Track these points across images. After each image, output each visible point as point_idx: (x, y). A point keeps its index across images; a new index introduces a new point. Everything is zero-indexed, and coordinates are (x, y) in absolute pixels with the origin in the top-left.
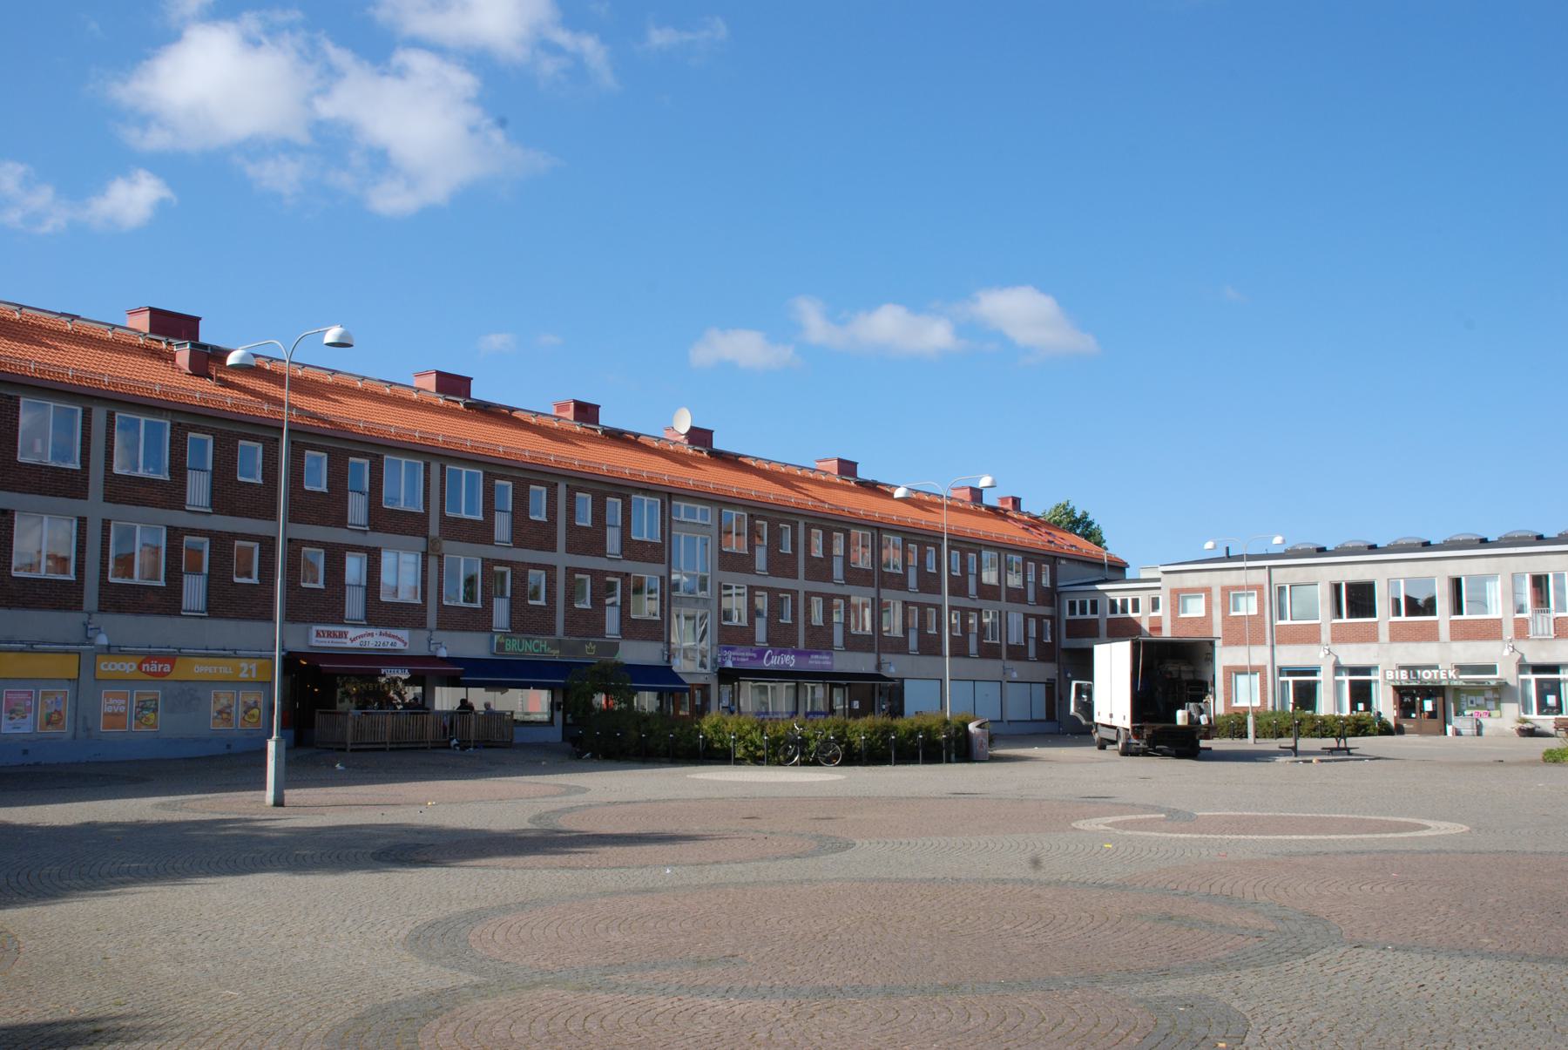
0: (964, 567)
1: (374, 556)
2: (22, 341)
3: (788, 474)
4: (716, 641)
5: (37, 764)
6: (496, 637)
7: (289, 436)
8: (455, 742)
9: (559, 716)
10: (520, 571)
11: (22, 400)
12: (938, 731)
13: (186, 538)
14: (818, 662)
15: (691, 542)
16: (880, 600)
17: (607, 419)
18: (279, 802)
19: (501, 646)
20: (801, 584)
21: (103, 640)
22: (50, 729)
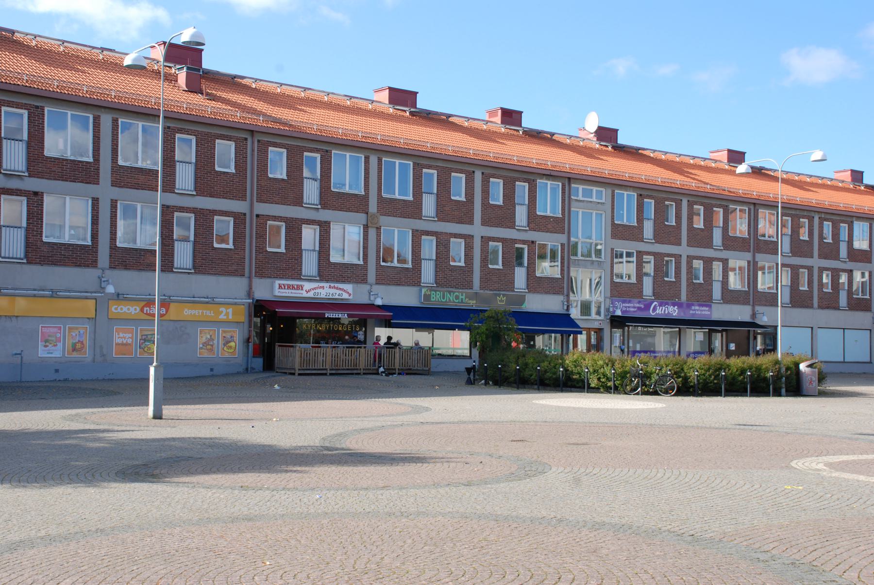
0: (836, 235)
1: (325, 228)
2: (279, 106)
3: (681, 163)
4: (609, 295)
5: (66, 380)
6: (424, 290)
7: (164, 122)
8: (382, 369)
9: (476, 353)
10: (204, 218)
11: (46, 109)
12: (767, 370)
13: (176, 214)
14: (699, 312)
15: (587, 217)
16: (755, 263)
17: (527, 122)
18: (158, 416)
19: (427, 297)
20: (816, 262)
21: (110, 289)
22: (75, 355)
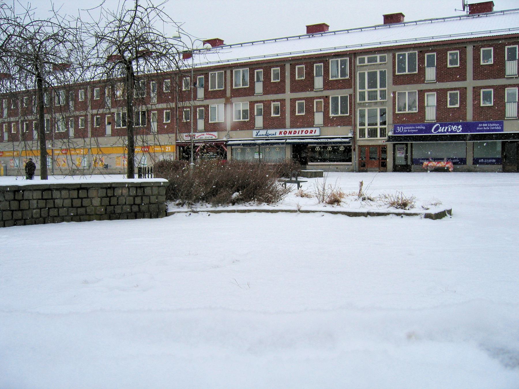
10: (267, 105)
